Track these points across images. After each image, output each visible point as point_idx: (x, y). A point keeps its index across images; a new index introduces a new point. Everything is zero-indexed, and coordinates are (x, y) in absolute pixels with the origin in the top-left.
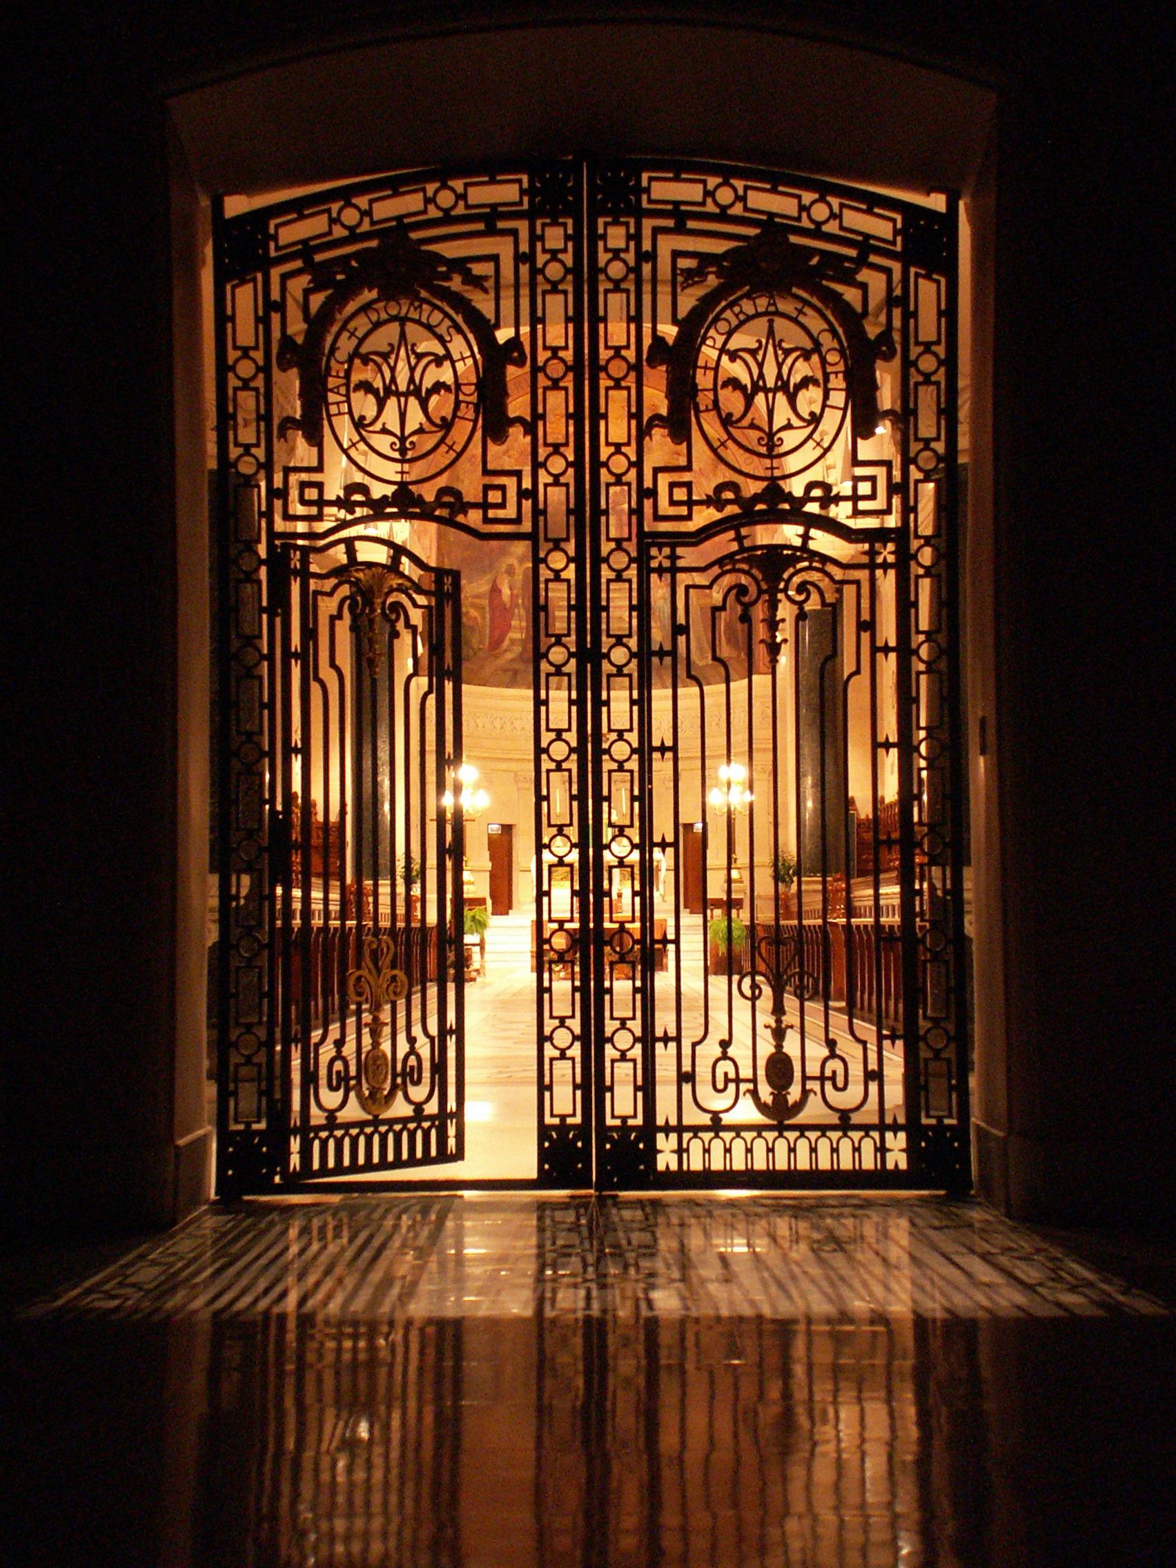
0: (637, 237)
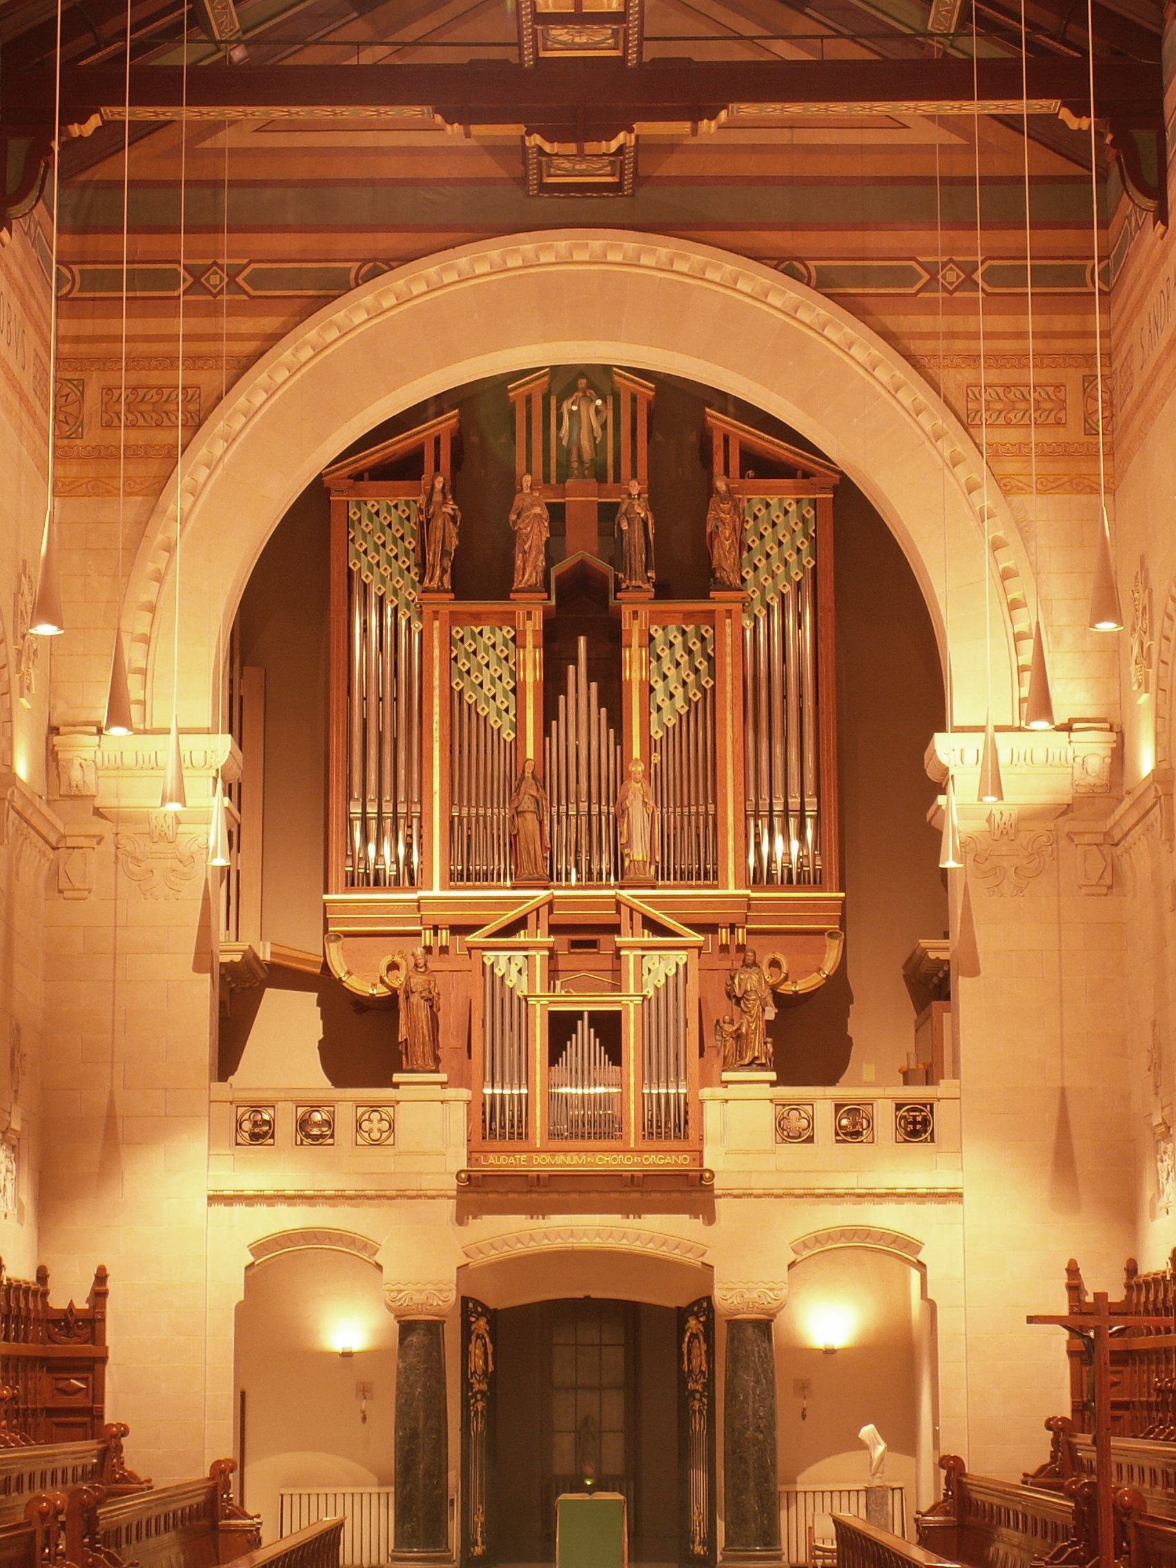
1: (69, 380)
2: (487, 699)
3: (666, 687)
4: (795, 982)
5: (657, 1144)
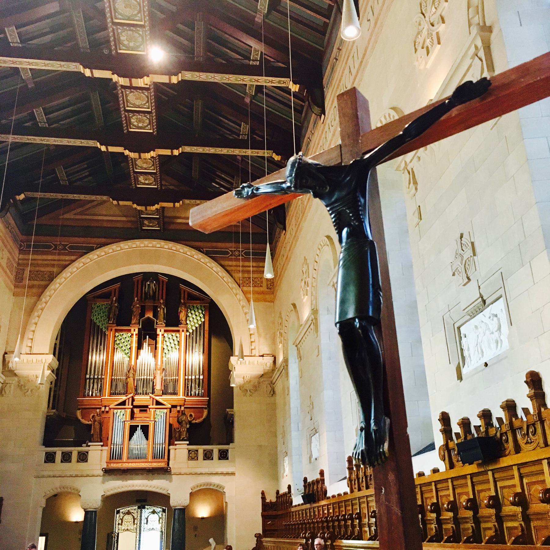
4: (196, 420)
5: (156, 460)
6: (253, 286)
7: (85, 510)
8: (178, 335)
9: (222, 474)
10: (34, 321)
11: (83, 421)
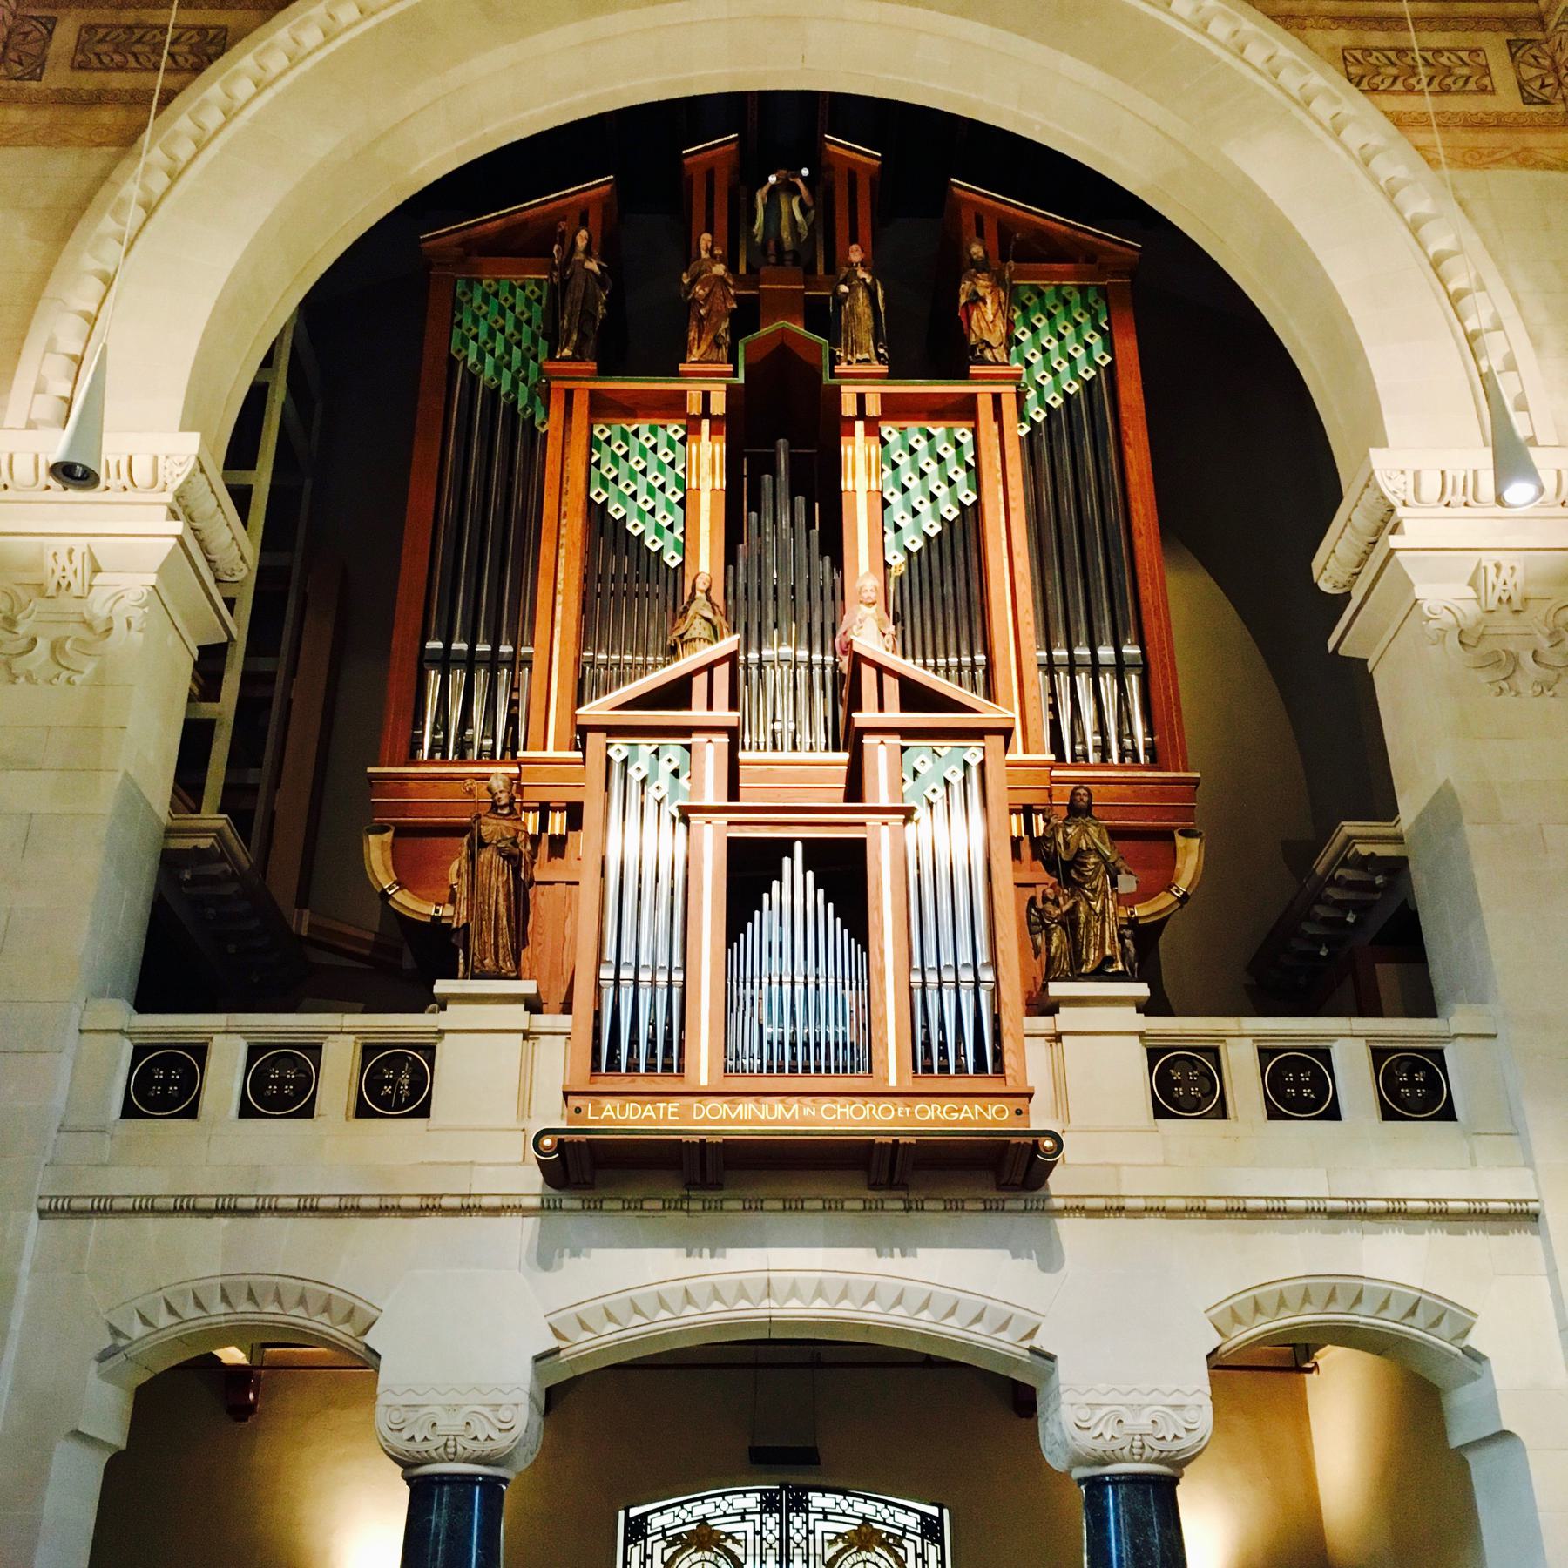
0: (806, 1523)
1: (33, 17)
2: (641, 514)
3: (907, 503)
6: (1435, 86)
7: (407, 1464)
8: (963, 432)
9: (1437, 1215)
10: (426, 1455)
11: (405, 901)
